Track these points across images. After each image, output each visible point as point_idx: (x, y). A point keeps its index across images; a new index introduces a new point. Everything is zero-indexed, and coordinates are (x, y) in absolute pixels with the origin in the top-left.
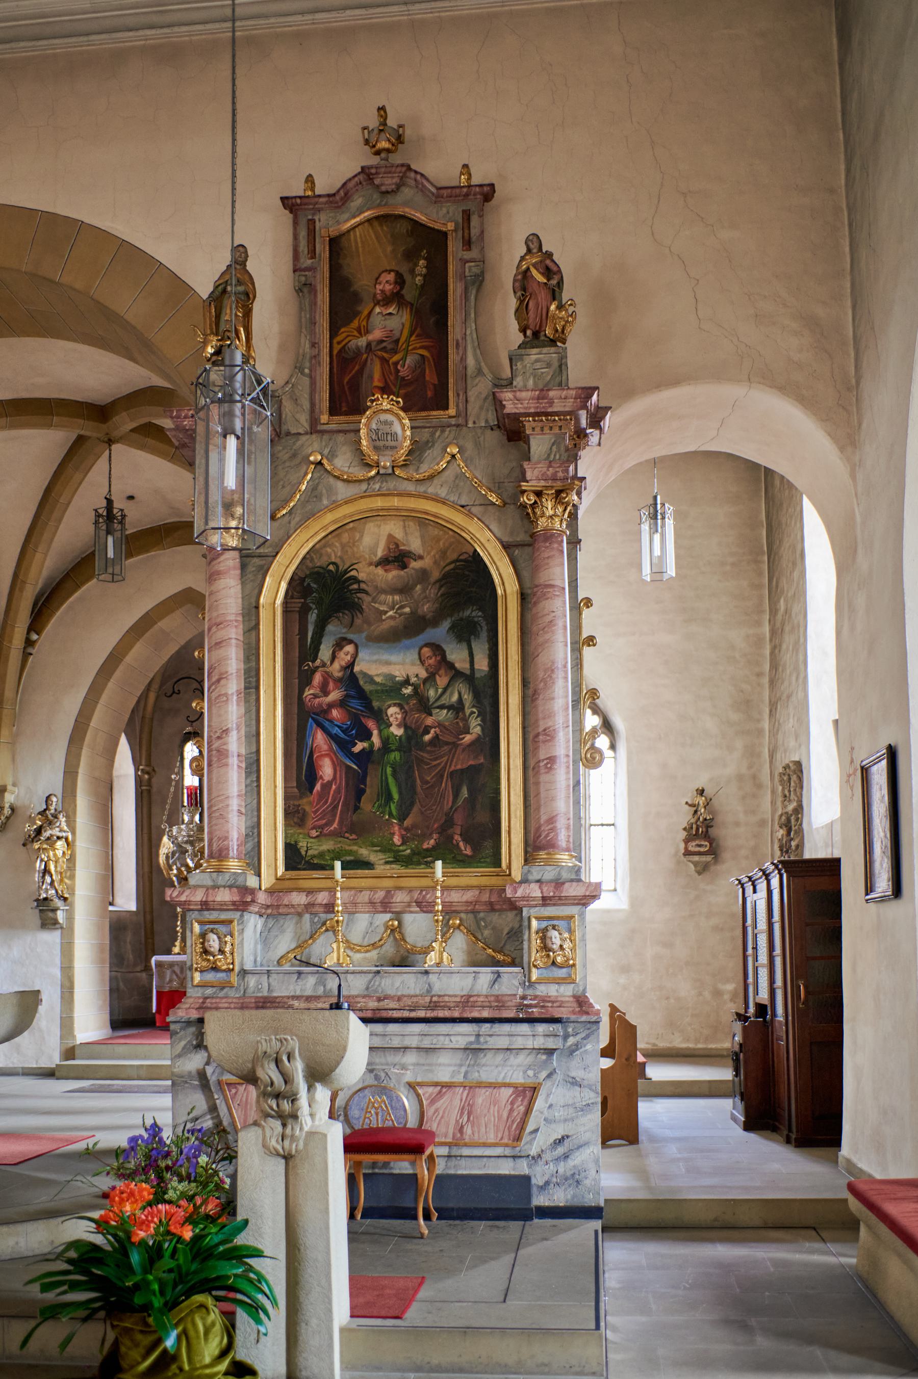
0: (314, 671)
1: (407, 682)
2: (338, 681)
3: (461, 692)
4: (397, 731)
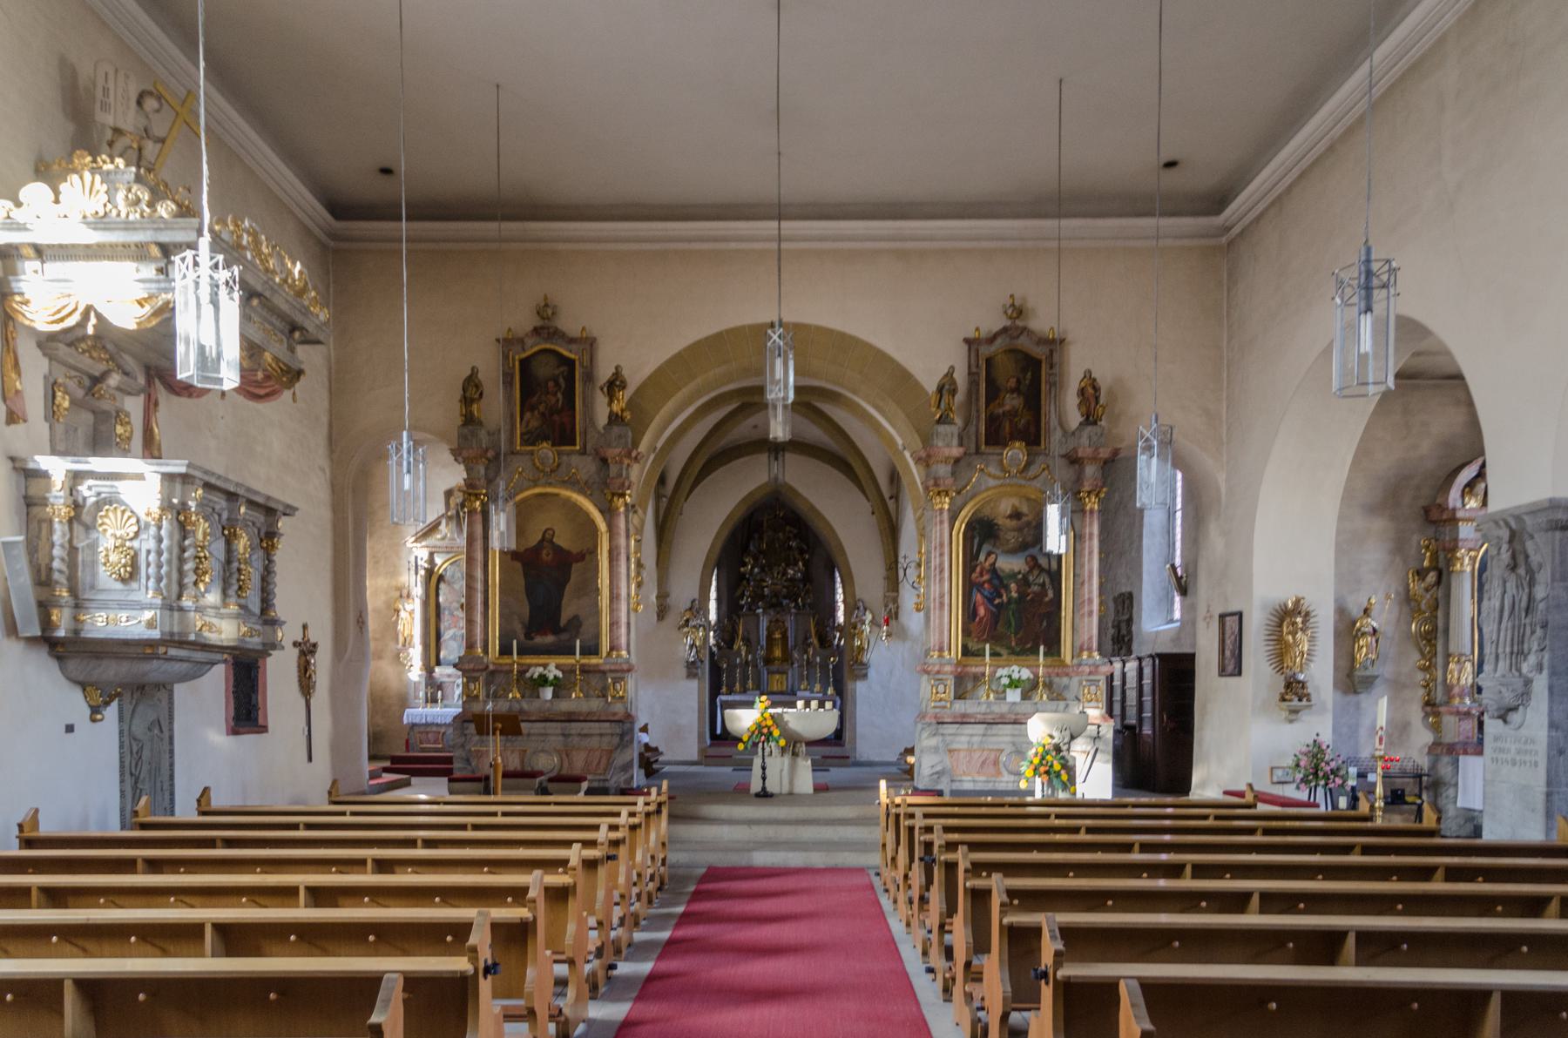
3: (1044, 578)
4: (1014, 595)
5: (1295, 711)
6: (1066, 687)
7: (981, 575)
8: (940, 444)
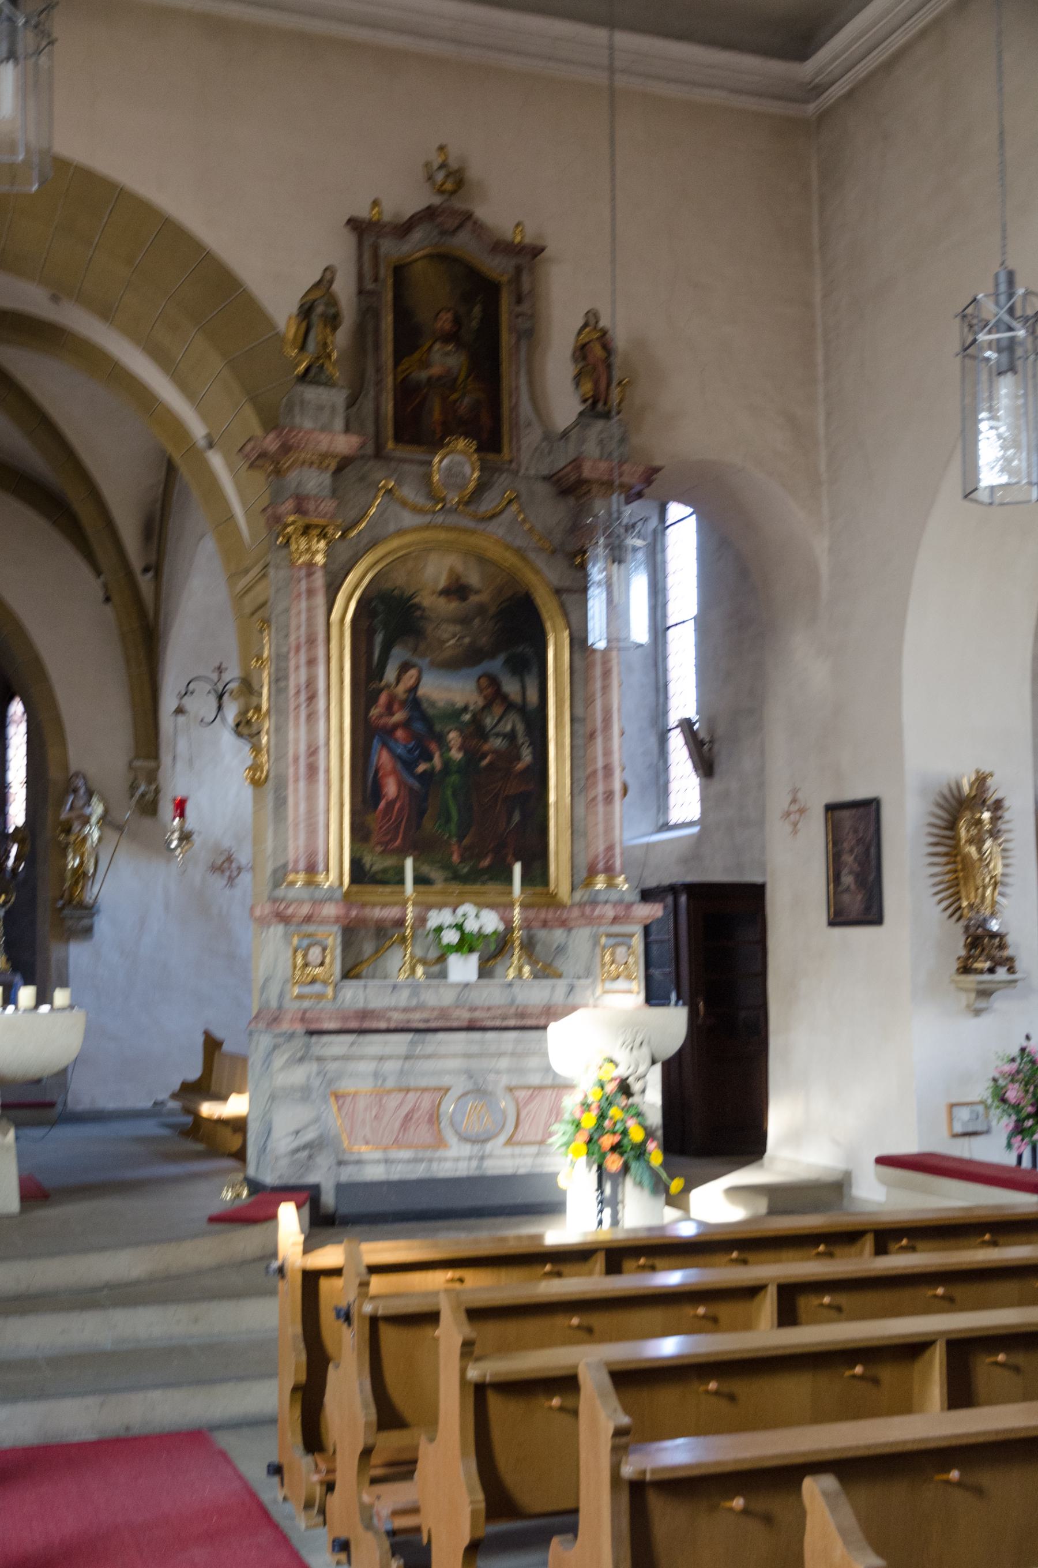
0: (381, 690)
1: (465, 709)
2: (403, 704)
3: (512, 723)
4: (456, 755)
5: (984, 993)
6: (561, 950)
7: (389, 710)
8: (308, 424)
